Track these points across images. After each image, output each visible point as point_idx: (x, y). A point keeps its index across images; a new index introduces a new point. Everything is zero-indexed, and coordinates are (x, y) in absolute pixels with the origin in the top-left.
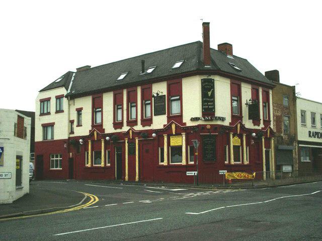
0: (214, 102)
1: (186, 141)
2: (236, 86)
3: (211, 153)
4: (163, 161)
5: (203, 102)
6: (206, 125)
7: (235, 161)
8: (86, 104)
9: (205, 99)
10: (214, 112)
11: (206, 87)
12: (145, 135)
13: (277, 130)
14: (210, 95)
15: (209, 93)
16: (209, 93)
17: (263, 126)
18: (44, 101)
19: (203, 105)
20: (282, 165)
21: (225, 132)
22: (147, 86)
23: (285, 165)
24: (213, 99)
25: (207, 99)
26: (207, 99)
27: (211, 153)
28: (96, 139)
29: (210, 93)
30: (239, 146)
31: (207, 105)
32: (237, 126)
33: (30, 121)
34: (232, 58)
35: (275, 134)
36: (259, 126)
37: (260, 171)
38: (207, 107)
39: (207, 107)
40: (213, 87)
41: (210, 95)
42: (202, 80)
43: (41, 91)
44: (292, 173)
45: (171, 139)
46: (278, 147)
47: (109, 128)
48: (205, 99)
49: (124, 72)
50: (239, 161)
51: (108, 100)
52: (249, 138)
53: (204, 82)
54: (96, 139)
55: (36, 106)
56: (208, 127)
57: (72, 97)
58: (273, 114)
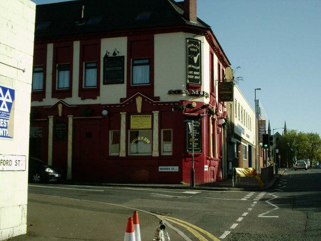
11: (191, 49)
14: (196, 61)
29: (196, 59)
31: (193, 75)
38: (192, 77)
39: (192, 77)
41: (196, 61)
48: (190, 66)
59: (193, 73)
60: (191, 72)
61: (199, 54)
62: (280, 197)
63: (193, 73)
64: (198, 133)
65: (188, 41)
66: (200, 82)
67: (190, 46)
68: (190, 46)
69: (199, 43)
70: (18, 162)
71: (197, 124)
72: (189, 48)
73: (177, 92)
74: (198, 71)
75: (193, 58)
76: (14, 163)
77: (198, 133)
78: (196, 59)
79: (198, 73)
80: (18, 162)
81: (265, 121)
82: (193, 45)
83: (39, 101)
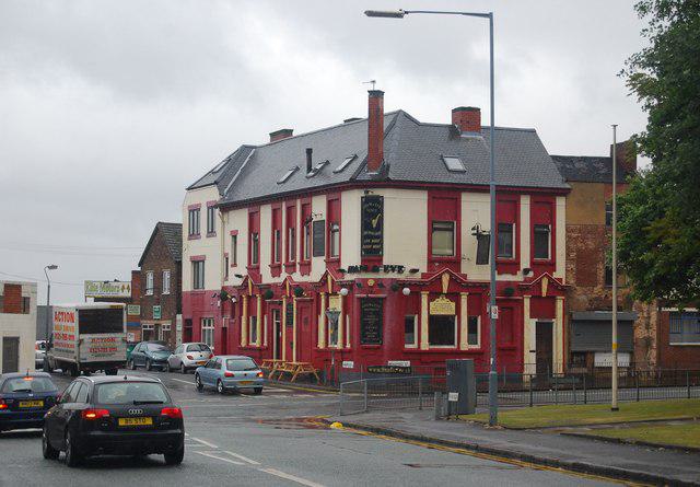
1: (421, 302)
4: (254, 341)
5: (364, 238)
6: (367, 279)
7: (432, 341)
8: (239, 220)
9: (366, 233)
12: (299, 289)
18: (194, 211)
20: (593, 353)
21: (407, 296)
22: (333, 196)
23: (601, 352)
28: (544, 295)
29: (374, 222)
30: (453, 317)
40: (381, 211)
43: (188, 189)
44: (628, 368)
45: (330, 301)
47: (267, 278)
48: (366, 233)
49: (464, 161)
50: (453, 344)
51: (266, 214)
52: (477, 307)
53: (366, 201)
54: (544, 295)
56: (371, 283)
57: (226, 208)
74: (378, 237)
78: (374, 222)
79: (377, 241)
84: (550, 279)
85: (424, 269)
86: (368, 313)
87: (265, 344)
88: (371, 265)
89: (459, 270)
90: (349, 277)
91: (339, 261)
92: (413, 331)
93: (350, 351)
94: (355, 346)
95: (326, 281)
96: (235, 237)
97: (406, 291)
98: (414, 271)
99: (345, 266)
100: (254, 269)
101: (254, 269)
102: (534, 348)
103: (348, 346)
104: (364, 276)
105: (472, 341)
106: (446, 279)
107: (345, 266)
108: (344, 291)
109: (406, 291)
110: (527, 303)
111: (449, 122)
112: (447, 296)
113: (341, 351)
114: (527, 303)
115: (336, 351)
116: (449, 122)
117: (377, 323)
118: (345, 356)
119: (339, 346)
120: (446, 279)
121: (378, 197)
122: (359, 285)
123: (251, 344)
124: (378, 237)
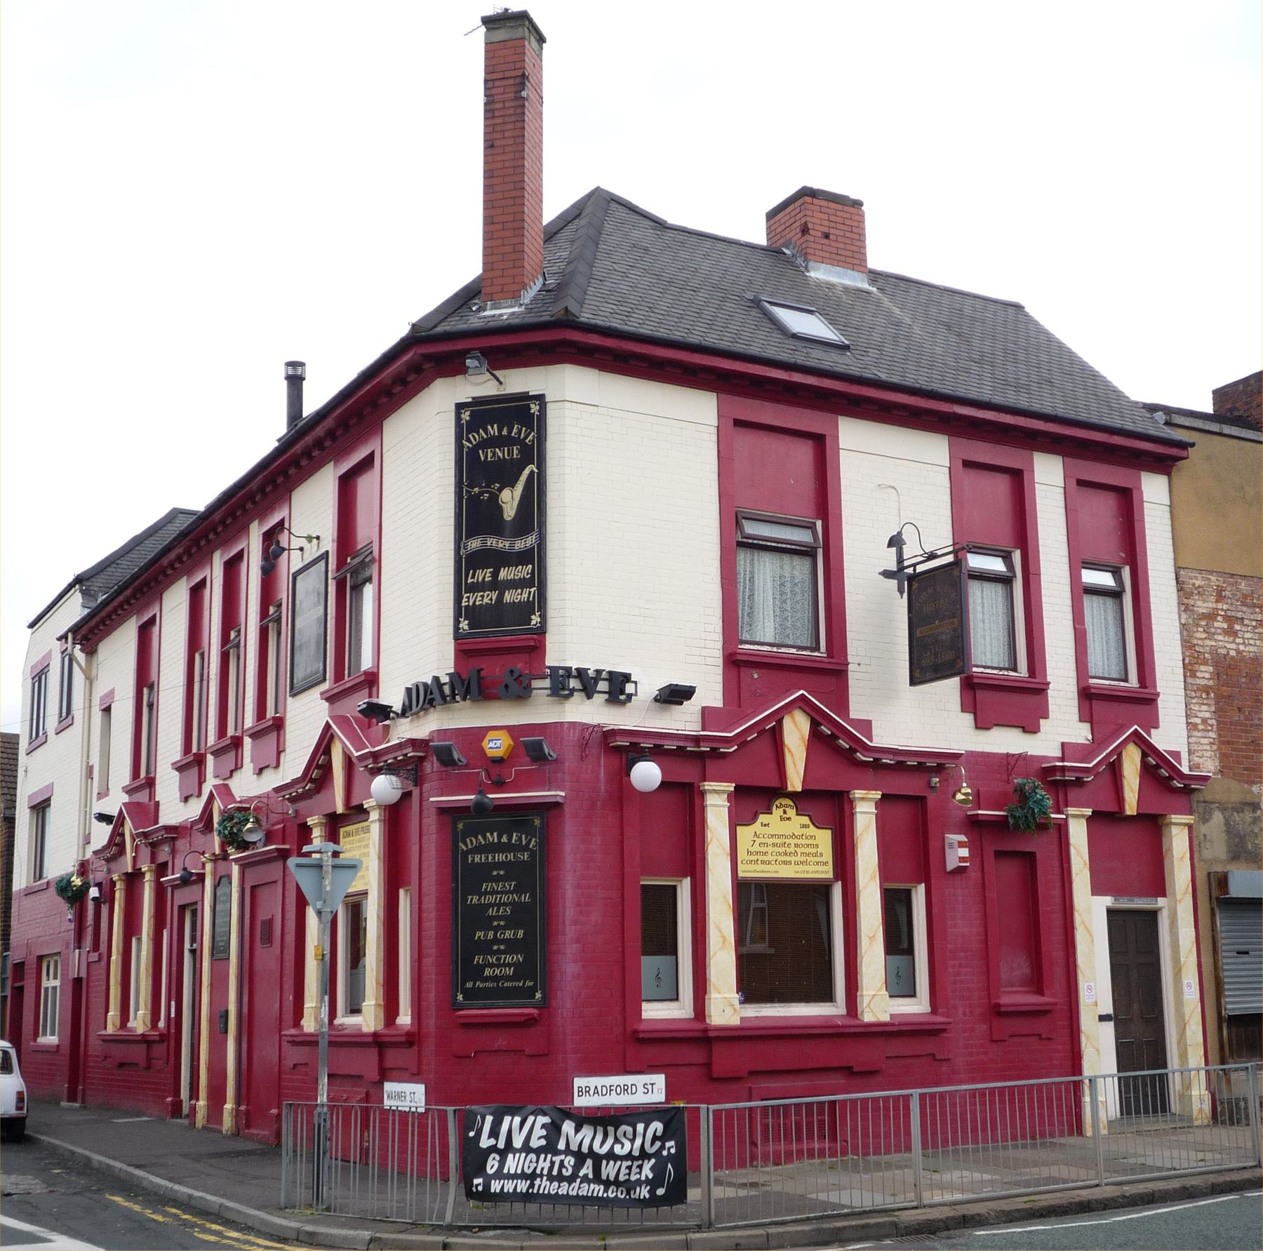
0: (536, 557)
2: (1000, 486)
3: (512, 946)
4: (355, 1010)
5: (466, 564)
7: (750, 989)
9: (474, 544)
10: (541, 631)
11: (487, 455)
13: (1223, 757)
14: (510, 512)
15: (506, 495)
16: (506, 495)
17: (1081, 734)
19: (461, 588)
24: (530, 541)
25: (493, 542)
26: (493, 542)
27: (512, 946)
28: (1131, 808)
29: (510, 500)
30: (820, 891)
31: (495, 585)
32: (775, 737)
33: (1131, 814)
34: (858, 281)
35: (1208, 792)
36: (1030, 728)
37: (308, 1099)
38: (489, 597)
39: (489, 597)
40: (535, 453)
41: (510, 512)
42: (460, 407)
46: (1222, 881)
48: (474, 544)
55: (24, 697)
56: (496, 745)
58: (1187, 644)
59: (495, 574)
60: (484, 575)
61: (531, 467)
62: (967, 1232)
63: (495, 574)
64: (526, 898)
65: (466, 416)
66: (535, 619)
67: (475, 438)
68: (475, 438)
69: (534, 408)
70: (649, 1087)
71: (519, 848)
72: (473, 452)
73: (943, 630)
74: (524, 557)
75: (495, 498)
76: (641, 1089)
77: (526, 898)
78: (510, 500)
79: (523, 572)
80: (649, 1087)
81: (1063, 744)
82: (493, 430)
83: (1025, 730)
84: (1148, 749)
85: (710, 693)
86: (483, 872)
87: (405, 1019)
88: (495, 669)
89: (842, 704)
90: (405, 730)
91: (371, 680)
92: (674, 951)
93: (412, 1039)
94: (431, 1023)
95: (327, 769)
96: (107, 710)
97: (647, 774)
98: (675, 695)
99: (391, 694)
100: (143, 782)
101: (143, 782)
102: (1108, 1009)
103: (405, 1019)
104: (465, 717)
105: (902, 985)
106: (796, 731)
107: (391, 694)
108: (384, 787)
109: (647, 774)
110: (1078, 834)
111: (758, 235)
112: (806, 800)
113: (377, 1042)
114: (1078, 834)
115: (356, 1041)
116: (758, 235)
117: (520, 916)
118: (393, 1058)
119: (368, 1020)
120: (796, 731)
121: (525, 397)
122: (445, 756)
123: (343, 1020)
124: (524, 557)
